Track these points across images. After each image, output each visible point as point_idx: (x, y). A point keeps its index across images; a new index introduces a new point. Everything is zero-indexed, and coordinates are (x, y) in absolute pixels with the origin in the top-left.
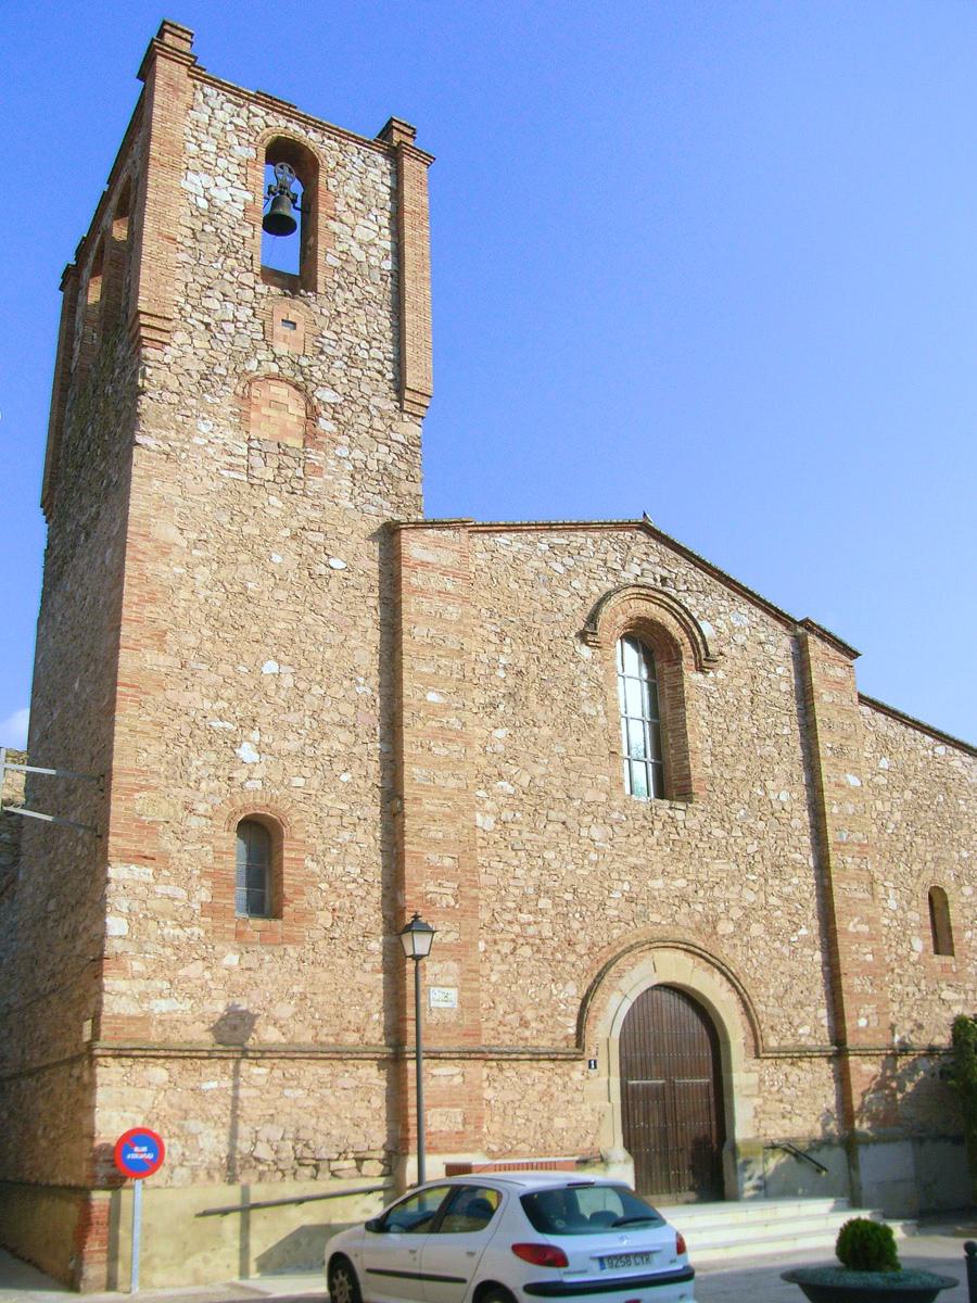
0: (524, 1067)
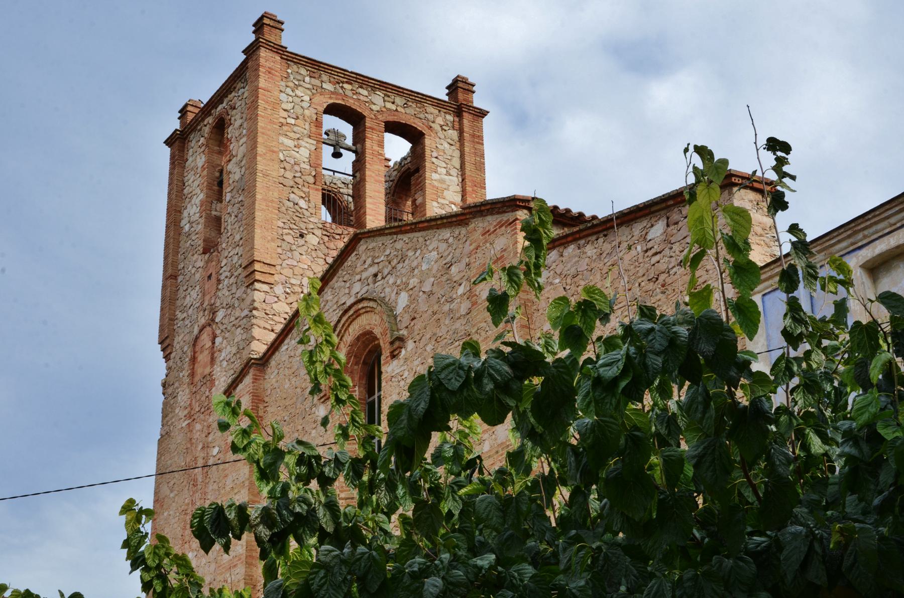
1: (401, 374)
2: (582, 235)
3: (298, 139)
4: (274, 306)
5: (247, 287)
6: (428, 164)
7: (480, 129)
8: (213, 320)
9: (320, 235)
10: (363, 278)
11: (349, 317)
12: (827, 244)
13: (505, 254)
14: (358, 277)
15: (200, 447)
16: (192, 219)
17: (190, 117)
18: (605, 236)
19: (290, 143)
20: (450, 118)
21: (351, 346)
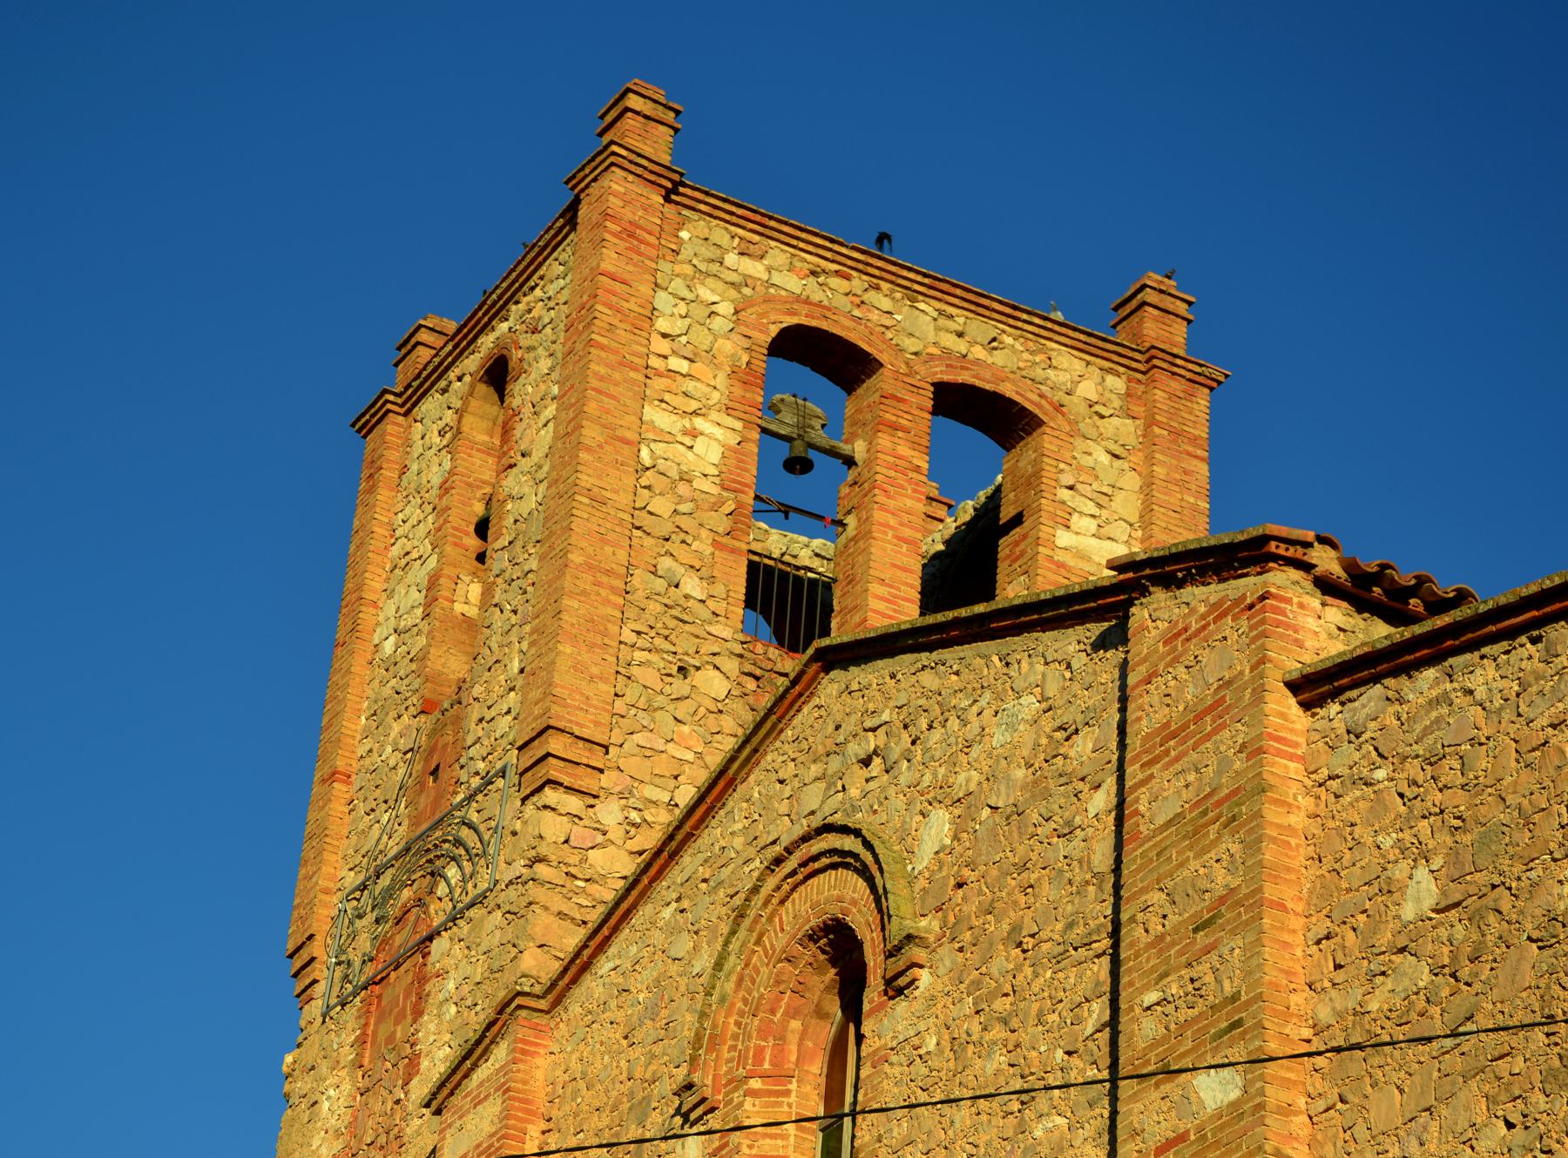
1: (916, 1041)
3: (694, 413)
9: (734, 673)
10: (830, 772)
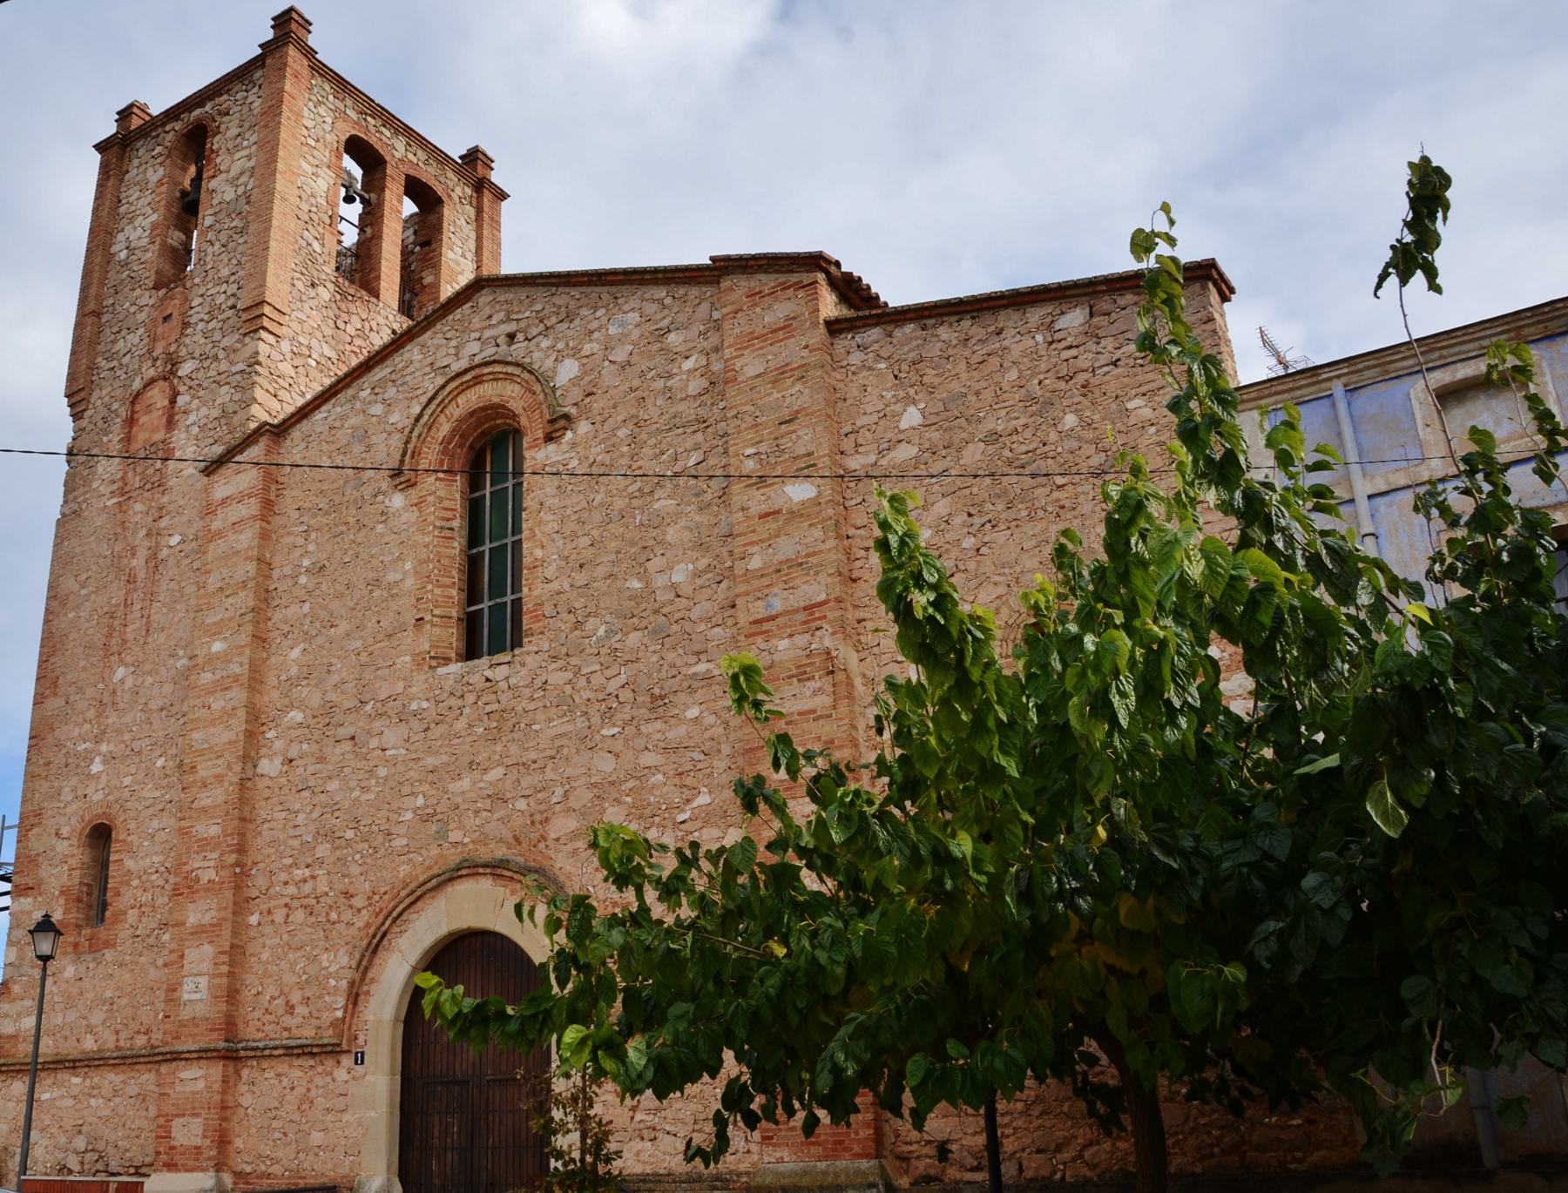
0: (282, 1067)
2: (933, 313)
4: (279, 364)
5: (245, 335)
6: (445, 238)
7: (499, 214)
8: (173, 373)
11: (462, 384)
12: (1388, 359)
13: (795, 324)
14: (477, 335)
15: (143, 532)
16: (133, 245)
17: (136, 122)
18: (973, 318)
19: (309, 169)
20: (468, 191)
21: (460, 421)
